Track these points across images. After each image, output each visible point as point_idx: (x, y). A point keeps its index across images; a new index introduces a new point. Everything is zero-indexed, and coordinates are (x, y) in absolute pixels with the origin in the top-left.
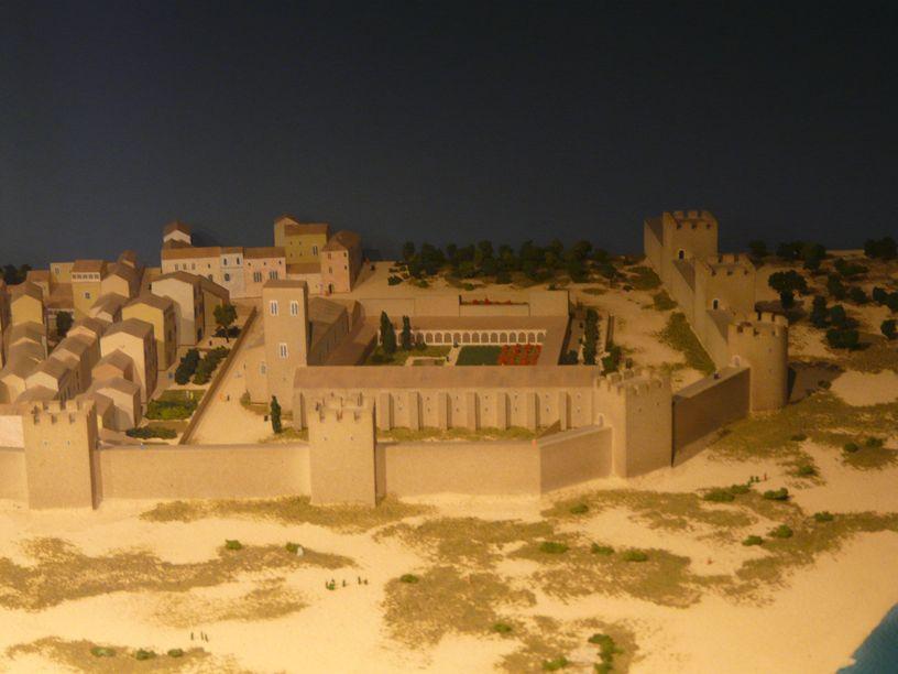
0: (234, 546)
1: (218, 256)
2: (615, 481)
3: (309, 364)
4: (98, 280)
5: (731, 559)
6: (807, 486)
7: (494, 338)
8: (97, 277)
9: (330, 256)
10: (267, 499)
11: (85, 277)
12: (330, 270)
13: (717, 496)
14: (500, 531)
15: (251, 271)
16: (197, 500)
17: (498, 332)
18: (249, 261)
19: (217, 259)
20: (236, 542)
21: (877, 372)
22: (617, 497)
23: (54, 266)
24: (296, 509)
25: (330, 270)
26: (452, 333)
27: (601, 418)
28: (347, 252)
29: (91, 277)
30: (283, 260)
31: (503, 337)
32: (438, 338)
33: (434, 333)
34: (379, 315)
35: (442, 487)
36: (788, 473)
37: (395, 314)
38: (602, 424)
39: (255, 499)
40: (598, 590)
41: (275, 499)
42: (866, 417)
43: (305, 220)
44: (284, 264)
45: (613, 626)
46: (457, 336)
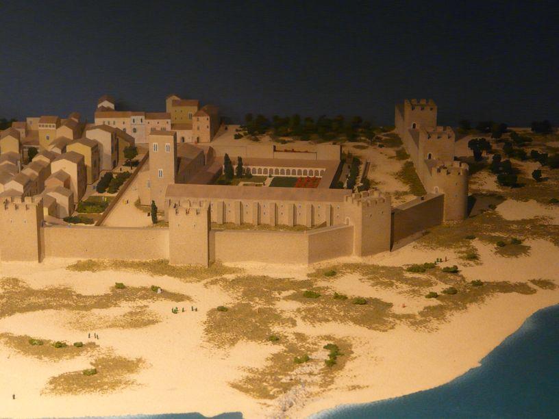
0: (120, 286)
1: (129, 117)
2: (354, 258)
3: (177, 182)
4: (55, 128)
5: (416, 305)
6: (471, 265)
7: (294, 172)
8: (54, 126)
9: (198, 120)
10: (144, 261)
11: (47, 126)
12: (198, 128)
13: (414, 269)
14: (280, 284)
15: (149, 127)
16: (101, 260)
17: (297, 169)
18: (148, 121)
19: (129, 119)
20: (122, 284)
21: (527, 201)
22: (354, 267)
23: (29, 120)
24: (160, 267)
25: (198, 128)
26: (269, 168)
27: (348, 220)
28: (209, 117)
29: (50, 126)
30: (169, 121)
31: (300, 172)
32: (260, 171)
33: (257, 168)
34: (224, 155)
35: (250, 257)
36: (460, 258)
37: (233, 155)
38: (348, 224)
39: (137, 260)
40: (334, 319)
41: (148, 261)
42: (515, 226)
43: (185, 97)
44: (170, 123)
45: (340, 340)
46: (271, 170)
